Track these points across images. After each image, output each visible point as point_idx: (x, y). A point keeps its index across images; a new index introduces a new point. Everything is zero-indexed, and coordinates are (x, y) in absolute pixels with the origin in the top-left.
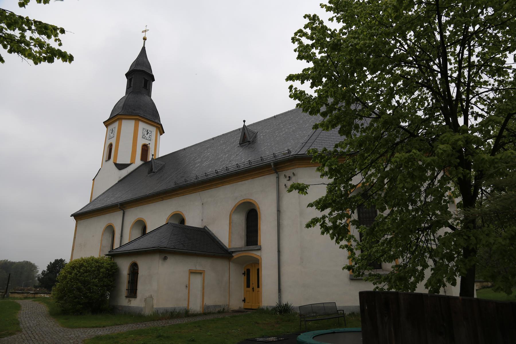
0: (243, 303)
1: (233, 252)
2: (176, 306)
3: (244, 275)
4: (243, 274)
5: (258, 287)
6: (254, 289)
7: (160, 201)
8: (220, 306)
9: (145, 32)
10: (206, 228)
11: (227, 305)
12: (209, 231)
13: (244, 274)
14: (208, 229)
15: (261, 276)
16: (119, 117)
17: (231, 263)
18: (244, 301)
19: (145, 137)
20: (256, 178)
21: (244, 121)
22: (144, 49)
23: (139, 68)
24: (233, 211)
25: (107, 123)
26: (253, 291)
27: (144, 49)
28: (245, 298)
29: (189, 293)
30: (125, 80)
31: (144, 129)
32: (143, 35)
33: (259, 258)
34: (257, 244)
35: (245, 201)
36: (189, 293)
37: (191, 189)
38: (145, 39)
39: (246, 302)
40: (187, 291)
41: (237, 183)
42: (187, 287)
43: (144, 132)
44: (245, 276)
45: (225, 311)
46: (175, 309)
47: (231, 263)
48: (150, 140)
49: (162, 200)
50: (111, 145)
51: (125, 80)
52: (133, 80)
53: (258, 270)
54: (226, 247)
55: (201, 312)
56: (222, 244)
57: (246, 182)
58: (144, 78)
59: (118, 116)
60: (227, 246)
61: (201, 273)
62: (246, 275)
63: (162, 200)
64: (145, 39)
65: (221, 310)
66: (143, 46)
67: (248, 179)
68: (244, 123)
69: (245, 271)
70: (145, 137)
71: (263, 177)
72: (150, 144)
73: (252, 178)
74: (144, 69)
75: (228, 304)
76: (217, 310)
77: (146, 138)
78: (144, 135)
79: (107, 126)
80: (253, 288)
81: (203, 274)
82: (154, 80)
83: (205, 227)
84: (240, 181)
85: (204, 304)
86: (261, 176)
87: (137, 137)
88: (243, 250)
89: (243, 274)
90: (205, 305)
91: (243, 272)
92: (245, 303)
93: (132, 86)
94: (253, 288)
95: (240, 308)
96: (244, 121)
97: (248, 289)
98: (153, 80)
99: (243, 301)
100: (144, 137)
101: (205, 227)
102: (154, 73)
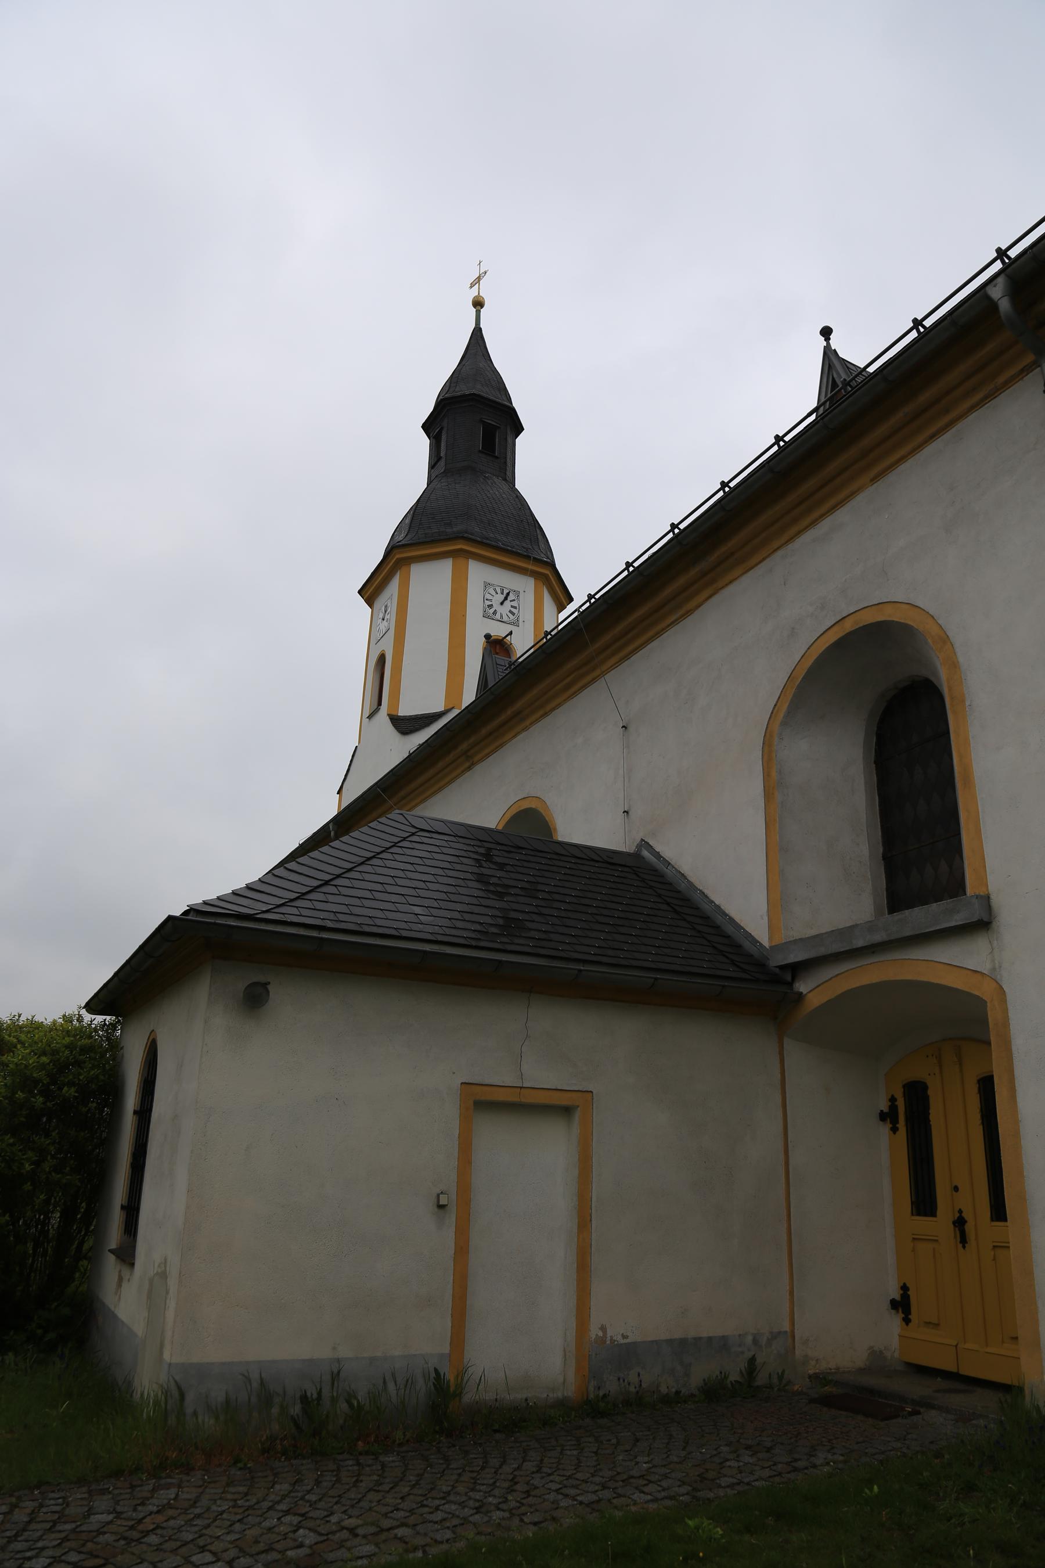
0: (894, 1322)
1: (797, 969)
2: (345, 1352)
3: (885, 1129)
4: (883, 1117)
5: (999, 1212)
6: (969, 1228)
7: (463, 772)
8: (721, 1345)
9: (479, 282)
10: (645, 853)
11: (775, 1336)
12: (660, 866)
13: (888, 1117)
14: (658, 855)
15: (1017, 1134)
16: (398, 556)
17: (789, 1044)
18: (902, 1305)
19: (495, 613)
20: (903, 467)
21: (826, 332)
22: (477, 338)
23: (464, 389)
24: (781, 715)
25: (370, 591)
26: (964, 1241)
27: (477, 338)
28: (905, 1288)
29: (462, 1250)
30: (424, 442)
31: (487, 585)
32: (474, 292)
33: (984, 991)
34: (956, 887)
35: (849, 626)
36: (462, 1250)
37: (569, 666)
38: (478, 304)
39: (913, 1316)
40: (449, 1234)
41: (790, 546)
42: (441, 1207)
43: (488, 596)
44: (894, 1130)
45: (761, 1380)
46: (335, 1376)
47: (789, 1044)
48: (516, 624)
49: (469, 768)
50: (382, 659)
51: (423, 443)
52: (444, 437)
53: (986, 1086)
54: (755, 941)
55: (570, 1390)
56: (730, 930)
57: (842, 515)
58: (482, 421)
59: (395, 551)
60: (764, 938)
61: (566, 1111)
62: (902, 1124)
63: (467, 764)
64: (478, 304)
65: (734, 1377)
66: (473, 326)
67: (853, 494)
68: (827, 339)
69: (893, 1099)
70: (495, 613)
71: (947, 436)
72: (511, 633)
73: (874, 480)
74: (479, 389)
75: (786, 1327)
76: (702, 1371)
77: (498, 616)
78: (490, 606)
79: (370, 602)
80: (960, 1223)
81: (577, 1116)
82: (518, 428)
83: (644, 844)
84: (806, 528)
85: (594, 1332)
86: (933, 437)
87: (464, 616)
88: (860, 943)
89: (883, 1117)
90: (601, 1341)
91: (884, 1106)
92: (907, 1321)
93: (442, 454)
94: (960, 1223)
95: (876, 1355)
96: (826, 332)
97: (923, 1223)
98: (518, 428)
99: (894, 1304)
100: (489, 613)
101: (644, 844)
102: (518, 404)
